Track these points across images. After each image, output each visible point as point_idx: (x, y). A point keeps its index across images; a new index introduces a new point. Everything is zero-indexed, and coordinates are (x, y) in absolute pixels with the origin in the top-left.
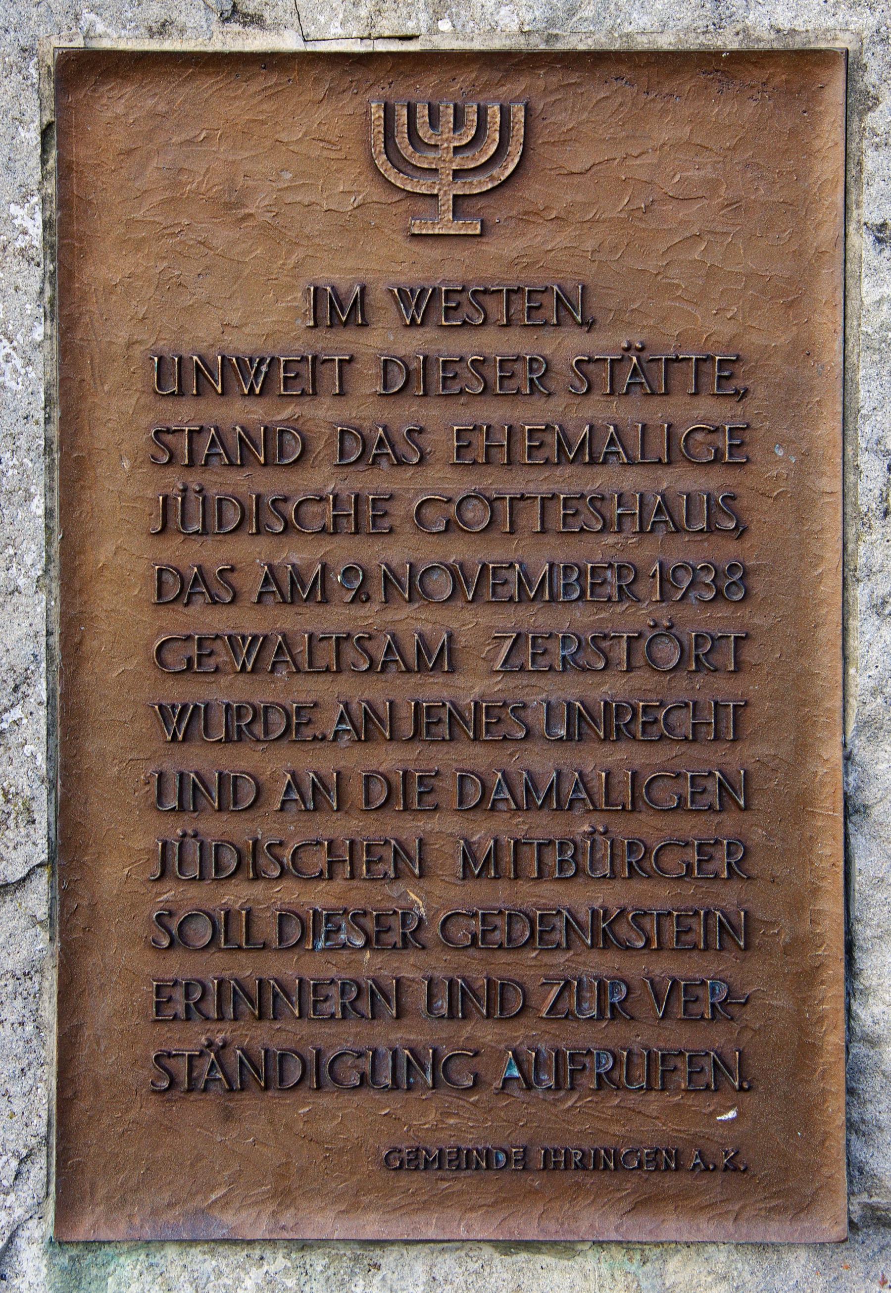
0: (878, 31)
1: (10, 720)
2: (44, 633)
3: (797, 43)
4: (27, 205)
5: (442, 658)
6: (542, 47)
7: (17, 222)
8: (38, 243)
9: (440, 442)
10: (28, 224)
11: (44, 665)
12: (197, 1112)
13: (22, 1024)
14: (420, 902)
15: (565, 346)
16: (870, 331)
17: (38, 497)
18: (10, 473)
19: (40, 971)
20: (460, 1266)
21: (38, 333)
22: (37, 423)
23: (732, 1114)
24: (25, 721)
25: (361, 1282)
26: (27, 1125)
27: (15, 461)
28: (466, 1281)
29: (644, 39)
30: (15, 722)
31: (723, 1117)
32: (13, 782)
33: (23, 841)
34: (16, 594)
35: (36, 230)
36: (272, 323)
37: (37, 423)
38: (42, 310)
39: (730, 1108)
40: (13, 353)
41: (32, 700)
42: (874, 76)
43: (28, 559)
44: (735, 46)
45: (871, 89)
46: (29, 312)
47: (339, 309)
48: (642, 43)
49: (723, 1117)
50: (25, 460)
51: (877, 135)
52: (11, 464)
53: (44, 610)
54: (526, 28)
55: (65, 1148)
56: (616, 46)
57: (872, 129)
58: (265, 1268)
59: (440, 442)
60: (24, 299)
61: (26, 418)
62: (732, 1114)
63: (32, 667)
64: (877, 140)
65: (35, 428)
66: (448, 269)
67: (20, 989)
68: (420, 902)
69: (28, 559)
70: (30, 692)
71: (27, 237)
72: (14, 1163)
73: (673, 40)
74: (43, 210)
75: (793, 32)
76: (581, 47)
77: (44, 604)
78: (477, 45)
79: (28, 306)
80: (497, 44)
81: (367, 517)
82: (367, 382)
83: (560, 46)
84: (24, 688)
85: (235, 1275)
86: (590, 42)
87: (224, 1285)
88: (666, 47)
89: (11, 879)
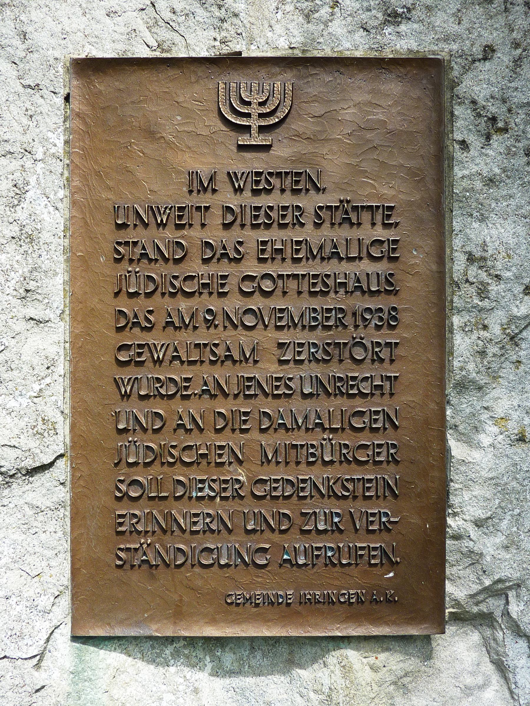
0: (458, 52)
1: (45, 384)
2: (63, 341)
3: (420, 56)
4: (56, 133)
5: (252, 358)
6: (300, 55)
7: (51, 141)
8: (61, 151)
9: (250, 248)
10: (57, 142)
11: (62, 357)
12: (135, 577)
13: (55, 532)
14: (243, 474)
15: (309, 202)
16: (458, 192)
17: (60, 274)
18: (46, 261)
19: (64, 507)
20: (265, 643)
21: (61, 193)
22: (60, 238)
23: (391, 575)
24: (52, 384)
25: (220, 650)
26: (58, 581)
27: (49, 256)
28: (268, 649)
29: (349, 53)
30: (48, 384)
31: (387, 576)
32: (46, 414)
33: (52, 443)
34: (50, 322)
35: (60, 144)
36: (171, 193)
37: (60, 238)
38: (62, 183)
39: (390, 572)
40: (49, 203)
41: (56, 374)
42: (457, 73)
43: (55, 305)
44: (391, 56)
45: (455, 79)
46: (56, 184)
47: (202, 185)
48: (347, 54)
49: (387, 576)
50: (53, 256)
51: (460, 98)
52: (47, 257)
53: (63, 330)
54: (292, 46)
55: (76, 592)
56: (335, 55)
57: (457, 96)
58: (175, 645)
59: (250, 248)
60: (54, 177)
61: (54, 235)
62: (391, 575)
63: (56, 358)
64: (460, 100)
65: (59, 240)
66: (257, 163)
67: (54, 516)
68: (243, 474)
69: (55, 305)
70: (55, 370)
71: (56, 148)
72: (52, 599)
73: (362, 53)
74: (64, 135)
75: (418, 52)
76: (319, 56)
77: (63, 327)
78: (269, 54)
79: (55, 181)
80: (278, 54)
81: (217, 288)
82: (216, 219)
83: (308, 55)
84: (52, 368)
85: (161, 648)
86: (323, 53)
87: (156, 653)
88: (358, 56)
89: (46, 463)
